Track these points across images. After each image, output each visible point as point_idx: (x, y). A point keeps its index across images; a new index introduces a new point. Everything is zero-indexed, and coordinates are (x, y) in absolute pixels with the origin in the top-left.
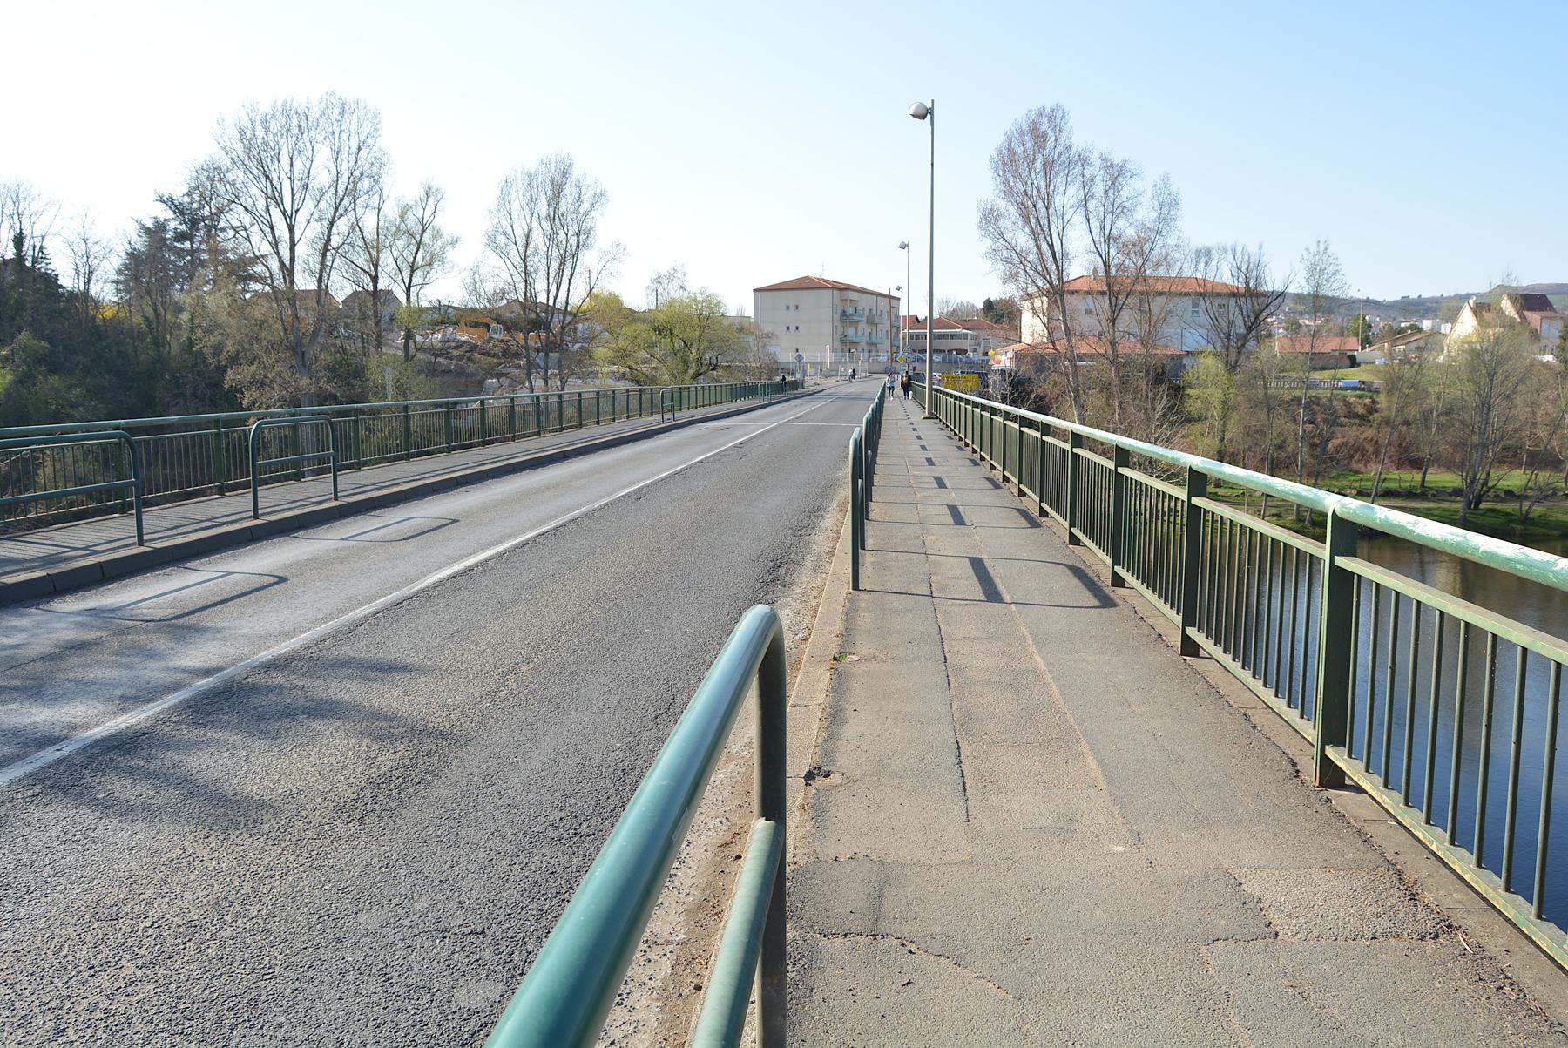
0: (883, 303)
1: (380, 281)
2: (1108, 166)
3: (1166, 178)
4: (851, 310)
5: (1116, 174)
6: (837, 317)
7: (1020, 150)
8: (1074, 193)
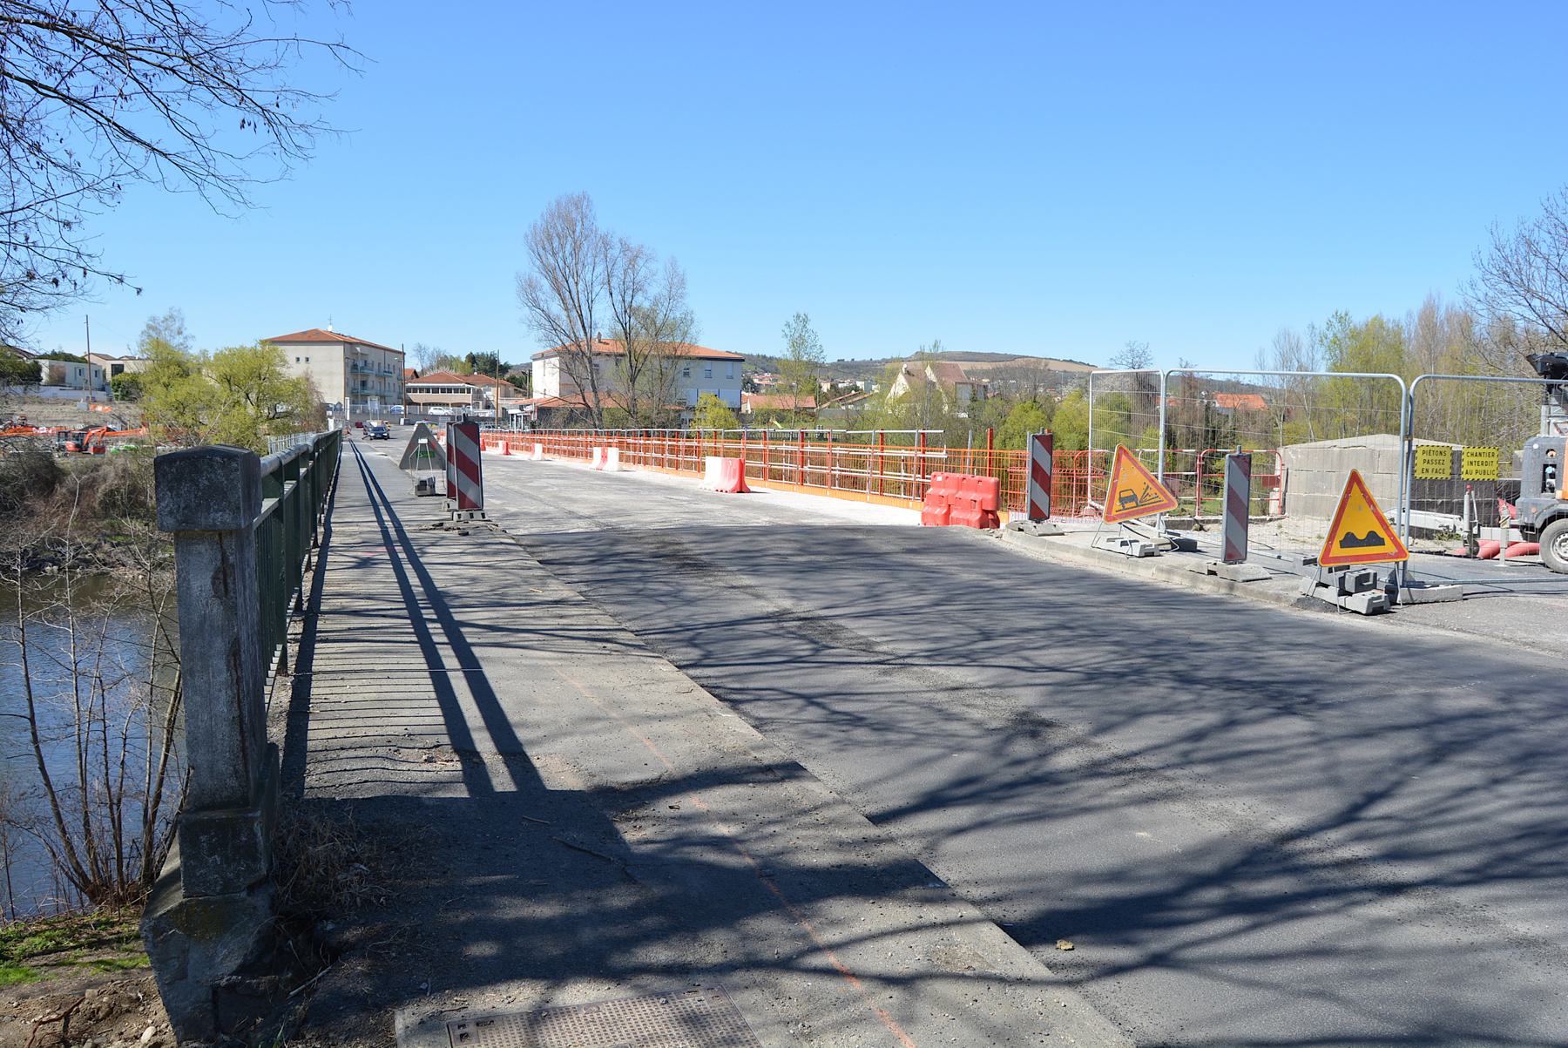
2: (625, 248)
3: (674, 263)
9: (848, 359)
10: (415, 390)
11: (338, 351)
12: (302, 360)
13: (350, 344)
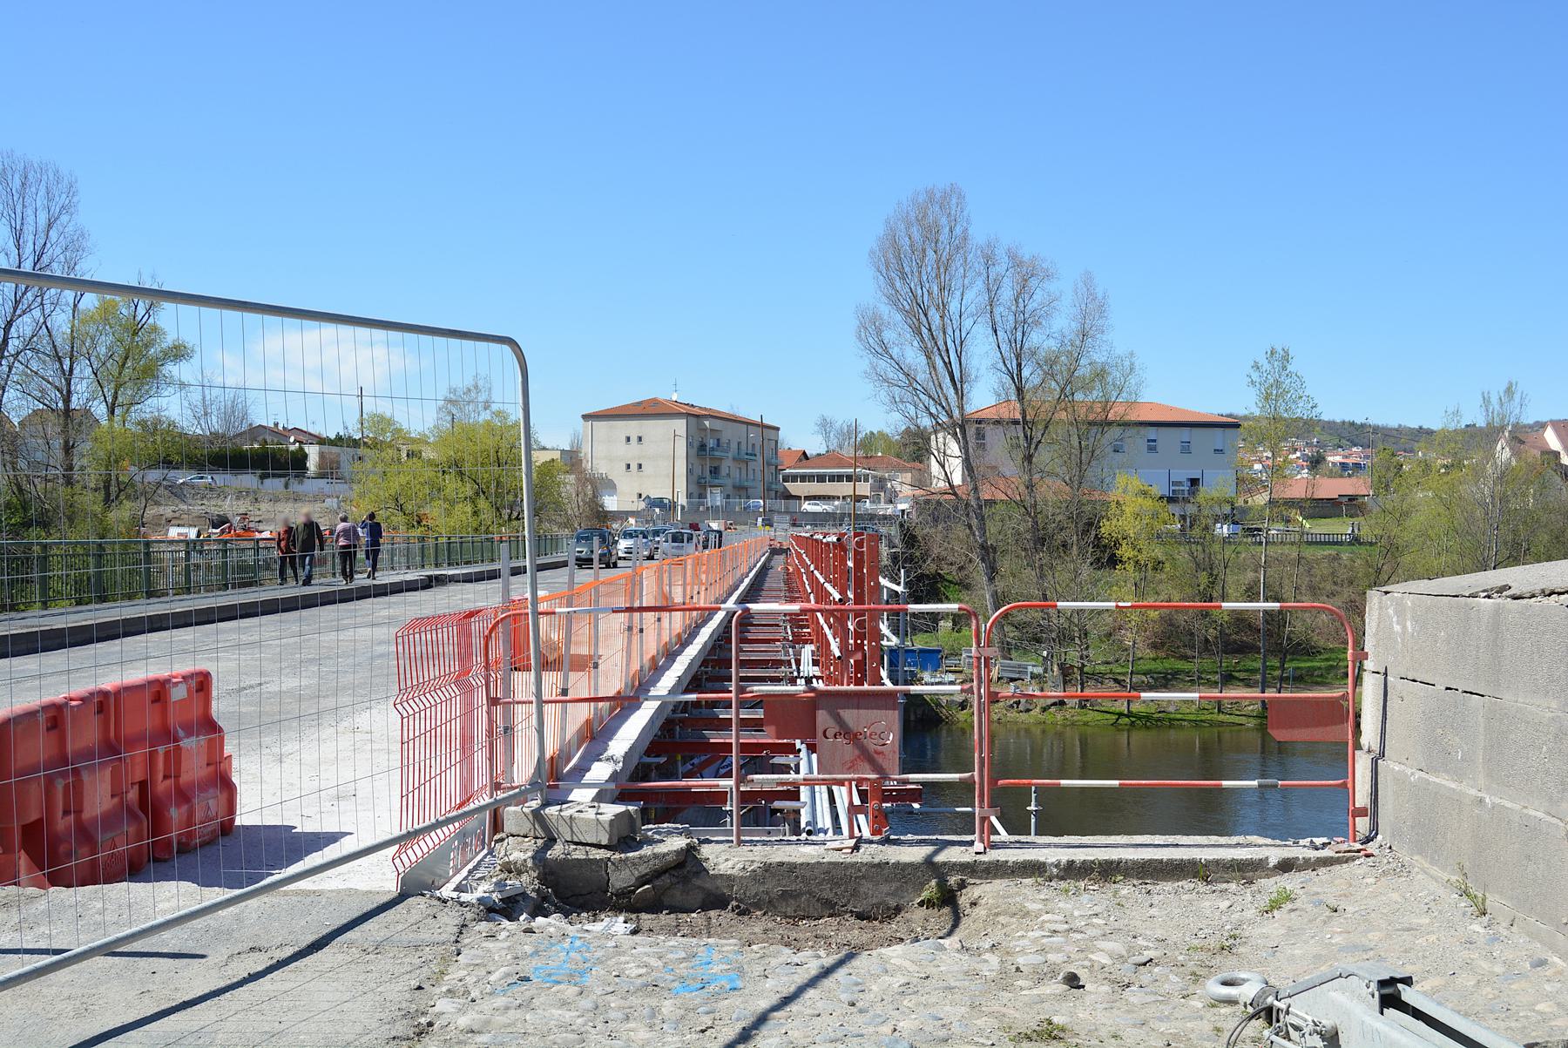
0: (753, 434)
1: (74, 398)
2: (1016, 262)
3: (1088, 280)
5: (1027, 275)
6: (694, 451)
7: (905, 243)
8: (975, 296)
9: (1358, 421)
10: (794, 478)
11: (680, 425)
12: (634, 439)
13: (694, 416)
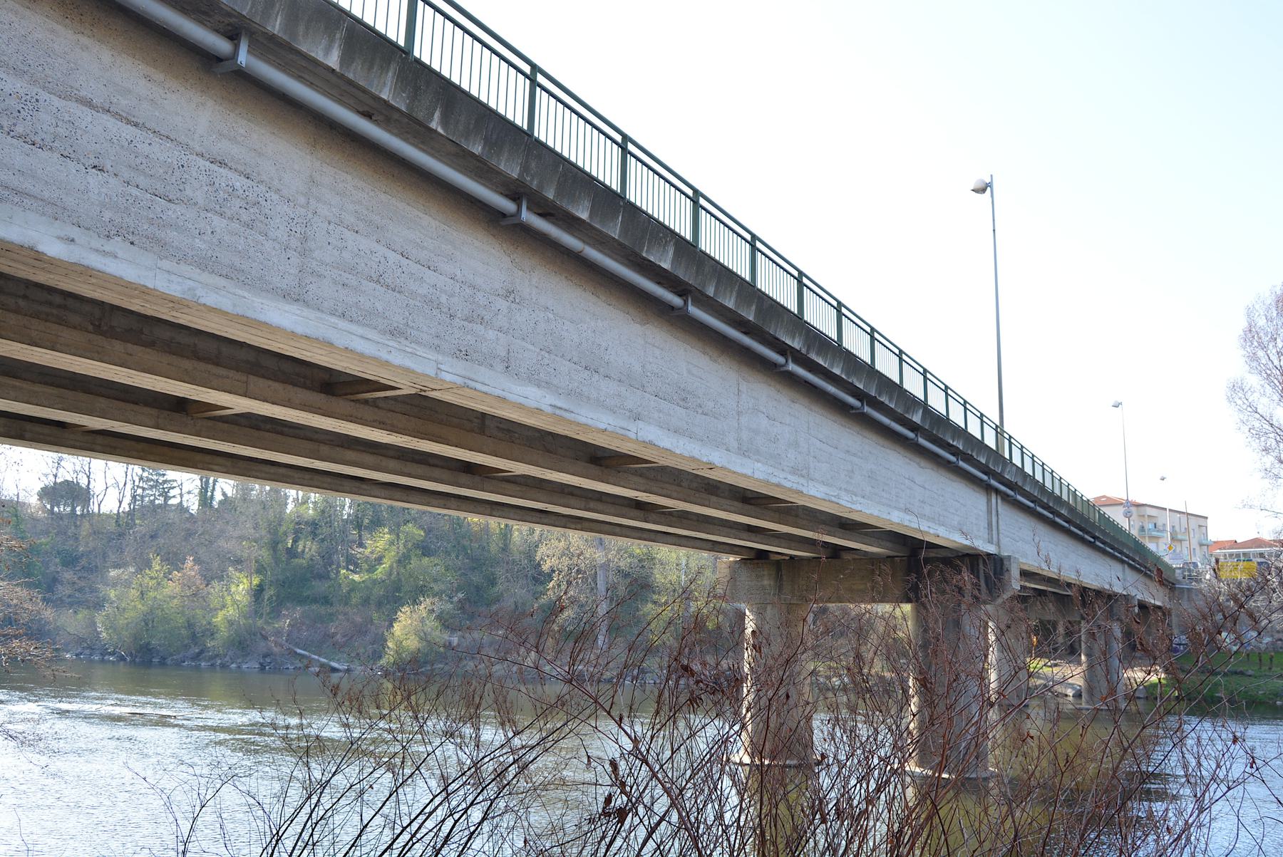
4: (1151, 526)
